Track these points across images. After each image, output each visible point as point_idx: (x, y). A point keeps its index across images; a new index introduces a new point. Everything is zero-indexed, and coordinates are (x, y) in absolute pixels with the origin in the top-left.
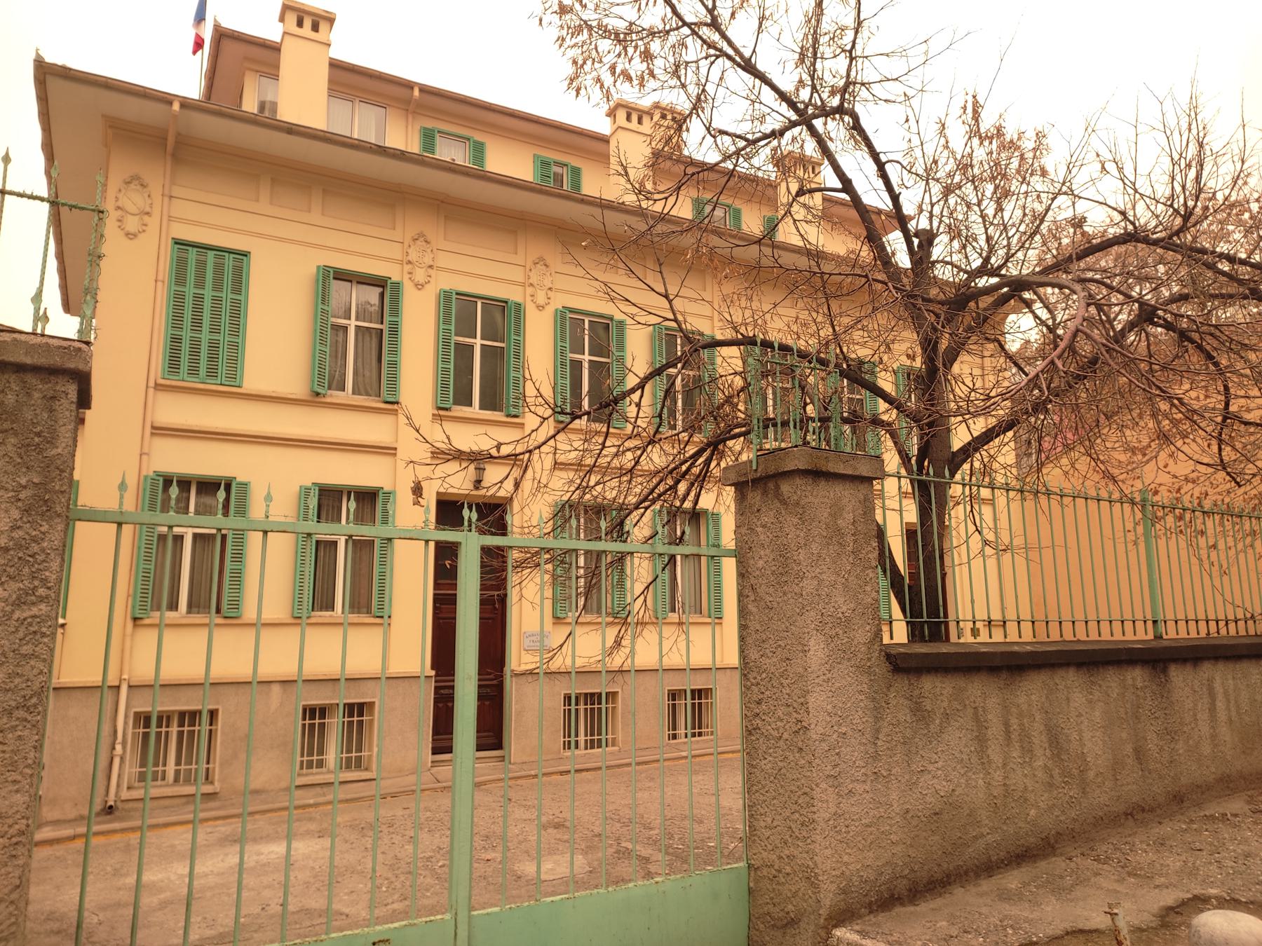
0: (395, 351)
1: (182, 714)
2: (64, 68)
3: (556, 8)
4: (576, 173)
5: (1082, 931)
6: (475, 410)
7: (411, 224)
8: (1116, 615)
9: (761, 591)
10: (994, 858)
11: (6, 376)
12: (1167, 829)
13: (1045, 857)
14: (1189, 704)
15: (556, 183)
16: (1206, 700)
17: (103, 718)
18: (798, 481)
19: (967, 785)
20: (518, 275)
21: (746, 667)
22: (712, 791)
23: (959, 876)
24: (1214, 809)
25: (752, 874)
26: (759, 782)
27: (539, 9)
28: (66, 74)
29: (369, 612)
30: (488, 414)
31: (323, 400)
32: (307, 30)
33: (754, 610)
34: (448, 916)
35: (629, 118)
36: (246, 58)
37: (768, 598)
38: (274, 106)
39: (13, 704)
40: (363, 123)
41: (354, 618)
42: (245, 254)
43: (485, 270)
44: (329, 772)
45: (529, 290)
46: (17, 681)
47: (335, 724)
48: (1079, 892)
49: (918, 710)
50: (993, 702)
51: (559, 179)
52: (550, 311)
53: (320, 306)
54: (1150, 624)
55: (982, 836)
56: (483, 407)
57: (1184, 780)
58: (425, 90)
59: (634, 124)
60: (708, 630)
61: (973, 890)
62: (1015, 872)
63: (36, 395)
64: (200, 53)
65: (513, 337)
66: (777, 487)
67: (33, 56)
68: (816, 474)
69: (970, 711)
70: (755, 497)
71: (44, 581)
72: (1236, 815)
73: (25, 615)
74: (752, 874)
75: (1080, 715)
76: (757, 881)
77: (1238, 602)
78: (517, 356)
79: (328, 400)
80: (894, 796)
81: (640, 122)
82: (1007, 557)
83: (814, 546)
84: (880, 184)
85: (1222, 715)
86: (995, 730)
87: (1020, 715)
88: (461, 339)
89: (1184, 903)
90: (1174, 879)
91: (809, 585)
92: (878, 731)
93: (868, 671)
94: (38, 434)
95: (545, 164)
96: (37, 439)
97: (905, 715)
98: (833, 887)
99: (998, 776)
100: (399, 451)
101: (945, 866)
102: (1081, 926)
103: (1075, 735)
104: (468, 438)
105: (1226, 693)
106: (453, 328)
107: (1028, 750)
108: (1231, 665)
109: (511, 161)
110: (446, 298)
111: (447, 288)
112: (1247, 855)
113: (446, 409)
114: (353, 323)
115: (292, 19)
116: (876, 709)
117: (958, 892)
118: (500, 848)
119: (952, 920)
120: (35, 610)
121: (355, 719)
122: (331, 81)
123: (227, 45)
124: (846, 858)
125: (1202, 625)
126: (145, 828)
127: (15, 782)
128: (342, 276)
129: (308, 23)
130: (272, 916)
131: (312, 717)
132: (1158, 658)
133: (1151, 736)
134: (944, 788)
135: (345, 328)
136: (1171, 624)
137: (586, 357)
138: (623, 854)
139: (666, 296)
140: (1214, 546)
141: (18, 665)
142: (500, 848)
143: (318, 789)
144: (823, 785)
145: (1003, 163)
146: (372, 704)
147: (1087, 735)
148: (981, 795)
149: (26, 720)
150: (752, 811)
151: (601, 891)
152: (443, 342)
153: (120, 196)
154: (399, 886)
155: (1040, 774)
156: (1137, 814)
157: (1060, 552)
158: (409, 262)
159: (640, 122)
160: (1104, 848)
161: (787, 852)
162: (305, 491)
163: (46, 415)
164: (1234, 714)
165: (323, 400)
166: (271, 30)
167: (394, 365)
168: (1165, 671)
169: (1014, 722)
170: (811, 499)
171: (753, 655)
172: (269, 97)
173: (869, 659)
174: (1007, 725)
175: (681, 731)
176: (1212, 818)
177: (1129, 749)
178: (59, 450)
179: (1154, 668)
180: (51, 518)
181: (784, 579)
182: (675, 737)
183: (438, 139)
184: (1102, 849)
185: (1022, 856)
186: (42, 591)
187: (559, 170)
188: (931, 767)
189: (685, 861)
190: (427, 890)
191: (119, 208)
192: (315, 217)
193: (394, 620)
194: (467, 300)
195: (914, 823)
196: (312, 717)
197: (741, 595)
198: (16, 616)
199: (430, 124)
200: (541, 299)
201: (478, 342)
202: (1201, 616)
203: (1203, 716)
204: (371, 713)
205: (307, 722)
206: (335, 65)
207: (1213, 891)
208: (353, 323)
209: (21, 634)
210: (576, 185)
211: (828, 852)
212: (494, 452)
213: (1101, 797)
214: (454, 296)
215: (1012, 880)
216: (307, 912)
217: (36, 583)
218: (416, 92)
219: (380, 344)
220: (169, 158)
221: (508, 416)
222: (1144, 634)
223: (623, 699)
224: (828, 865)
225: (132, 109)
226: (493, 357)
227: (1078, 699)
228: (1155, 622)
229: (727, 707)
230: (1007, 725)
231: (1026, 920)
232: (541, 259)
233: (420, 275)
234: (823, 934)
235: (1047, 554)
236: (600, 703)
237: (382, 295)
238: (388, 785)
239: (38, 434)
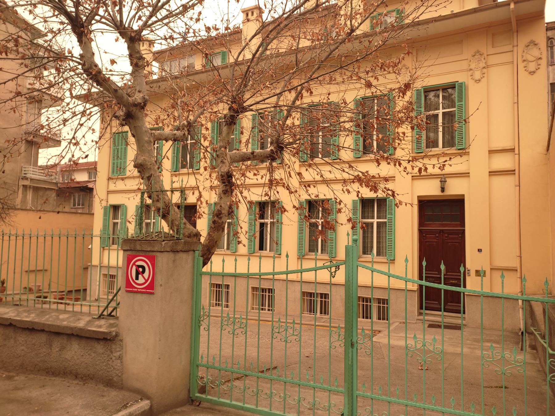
1: (321, 294)
17: (233, 288)
100: (471, 175)
191: (524, 61)
236: (314, 297)
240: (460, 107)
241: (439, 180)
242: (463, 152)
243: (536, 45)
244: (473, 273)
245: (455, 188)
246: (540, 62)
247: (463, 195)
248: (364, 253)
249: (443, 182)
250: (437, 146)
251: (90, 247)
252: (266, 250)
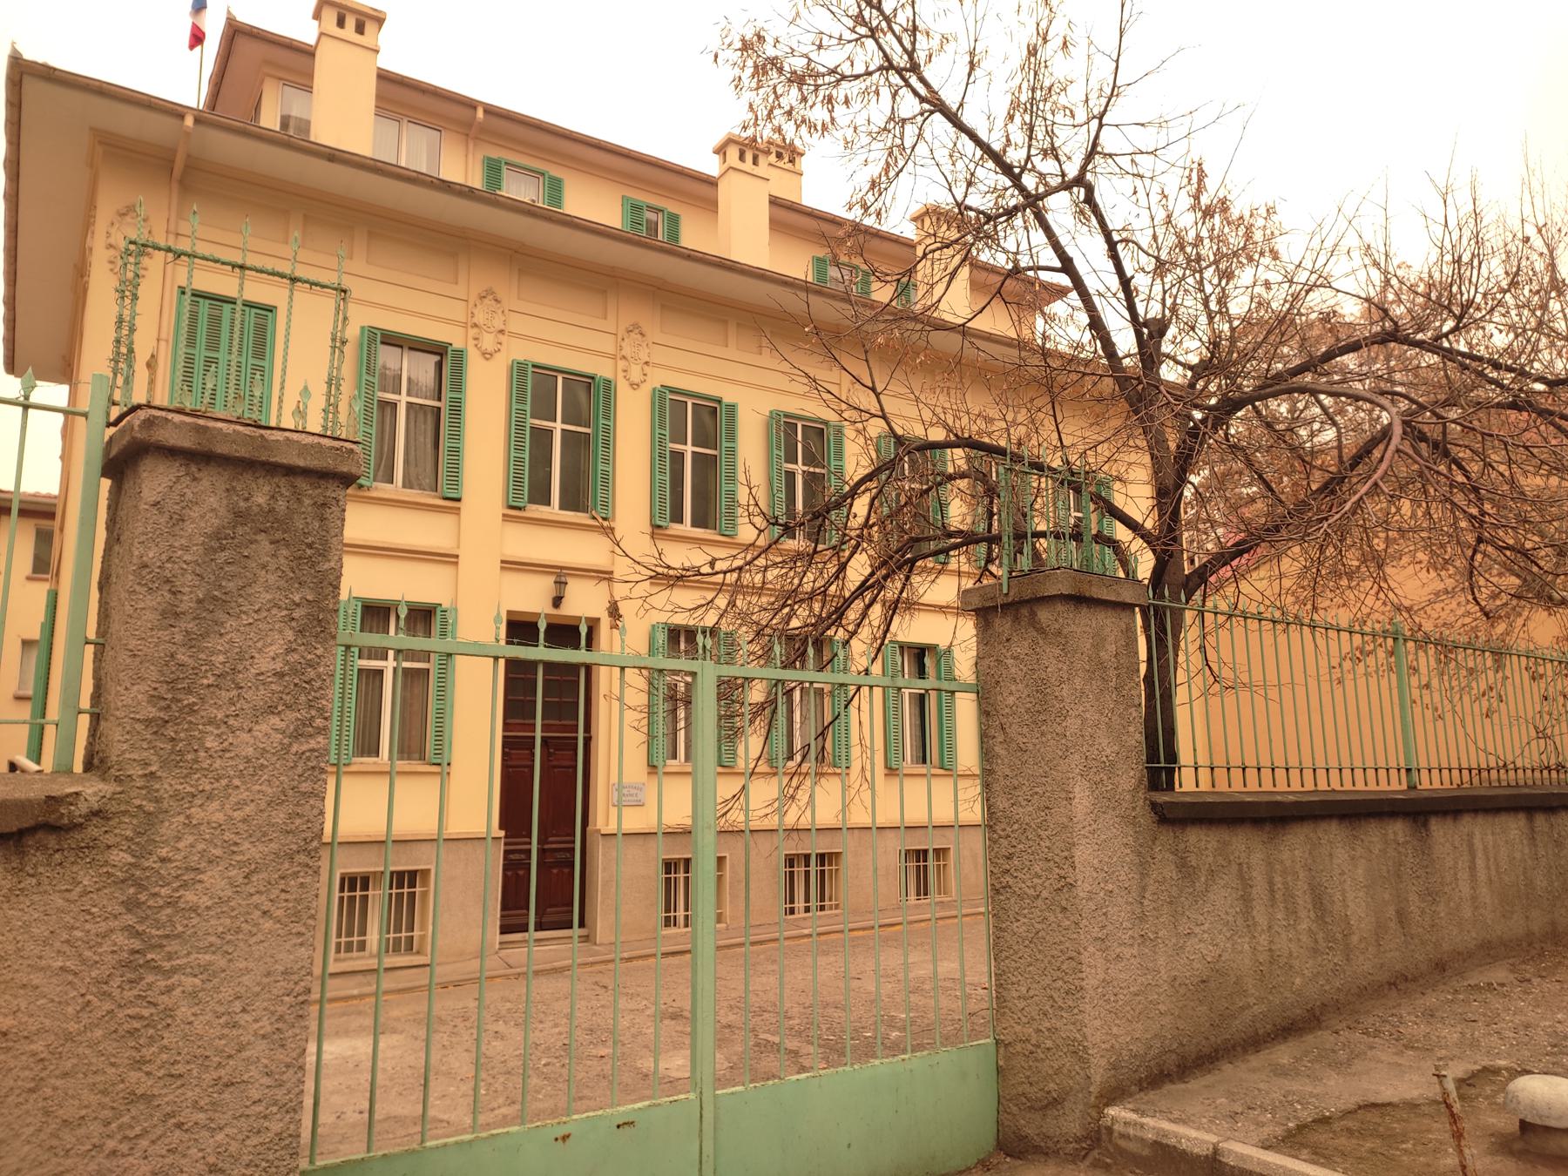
0: (457, 435)
2: (45, 66)
3: (739, 45)
4: (674, 220)
5: (1374, 1105)
6: (554, 510)
7: (478, 277)
8: (1370, 763)
9: (1013, 731)
10: (1261, 1032)
11: (276, 480)
12: (1431, 1000)
13: (1311, 1030)
14: (1449, 862)
15: (645, 232)
16: (1466, 857)
18: (1060, 607)
19: (1234, 949)
20: (608, 345)
21: (992, 819)
22: (951, 963)
23: (1227, 1050)
24: (1478, 978)
25: (1002, 1050)
26: (1010, 947)
27: (715, 45)
28: (49, 75)
29: (422, 757)
30: (699, 532)
31: (367, 494)
32: (349, 31)
33: (1003, 752)
34: (692, 1096)
35: (742, 158)
36: (268, 62)
37: (1021, 740)
38: (305, 126)
39: (294, 847)
40: (413, 149)
41: (402, 765)
42: (271, 309)
43: (570, 338)
44: (371, 956)
45: (621, 364)
46: (298, 821)
47: (378, 896)
48: (1358, 1065)
49: (1184, 867)
50: (1257, 858)
51: (653, 228)
52: (646, 390)
53: (365, 377)
54: (1403, 772)
55: (1249, 1006)
56: (694, 525)
57: (1446, 947)
58: (491, 111)
59: (748, 165)
61: (1243, 1066)
62: (1283, 1047)
63: (307, 502)
64: (198, 49)
65: (602, 421)
66: (1033, 614)
67: (7, 51)
68: (1079, 600)
69: (1235, 867)
70: (1003, 625)
71: (321, 710)
72: (1503, 985)
73: (304, 748)
74: (1002, 1050)
75: (1342, 873)
76: (1007, 1059)
77: (1491, 749)
78: (606, 445)
79: (374, 494)
80: (1161, 961)
81: (755, 162)
82: (1230, 698)
83: (1077, 680)
84: (1110, 266)
85: (1482, 875)
86: (1259, 889)
87: (1284, 872)
88: (537, 422)
89: (1474, 1075)
90: (1456, 1051)
91: (1073, 724)
92: (1144, 889)
93: (1133, 822)
94: (310, 546)
95: (636, 208)
96: (309, 552)
97: (1170, 872)
98: (1103, 1062)
99: (1263, 940)
100: (461, 560)
101: (1213, 1039)
102: (1372, 1100)
103: (1338, 896)
104: (679, 557)
105: (1485, 849)
106: (528, 408)
107: (1292, 912)
108: (1490, 819)
109: (594, 203)
110: (519, 370)
111: (521, 359)
112: (1527, 1027)
113: (519, 509)
114: (403, 399)
115: (330, 16)
116: (1141, 864)
117: (1227, 1068)
118: (610, 1043)
119: (1231, 1096)
120: (313, 744)
121: (406, 890)
122: (379, 97)
123: (243, 46)
124: (1115, 1030)
125: (1455, 773)
126: (531, 975)
127: (299, 934)
128: (392, 340)
129: (350, 22)
130: (354, 1126)
131: (352, 888)
132: (1418, 811)
133: (1413, 897)
134: (1211, 953)
135: (394, 405)
136: (1424, 773)
137: (689, 449)
138: (764, 1047)
139: (873, 389)
140: (1427, 686)
141: (298, 804)
142: (610, 1043)
143: (360, 978)
144: (1091, 949)
145: (1218, 240)
146: (425, 873)
147: (1350, 896)
148: (1247, 961)
149: (307, 865)
150: (1001, 981)
151: (848, 1068)
152: (515, 426)
153: (113, 231)
154: (500, 1088)
155: (1304, 938)
156: (1400, 983)
157: (1300, 691)
158: (475, 325)
159: (755, 162)
160: (1371, 1020)
161: (1048, 1025)
163: (317, 524)
164: (1493, 873)
165: (367, 494)
166: (304, 30)
167: (456, 452)
168: (1425, 824)
169: (1278, 879)
170: (1073, 628)
171: (1001, 803)
172: (295, 112)
173: (1134, 809)
174: (1271, 883)
175: (800, 904)
176: (1476, 988)
177: (1391, 911)
178: (332, 564)
179: (1415, 821)
180: (326, 640)
181: (1042, 717)
182: (792, 911)
183: (505, 171)
184: (1368, 1021)
185: (1288, 1030)
186: (319, 722)
187: (652, 216)
188: (1197, 930)
189: (843, 1054)
190: (538, 1092)
193: (454, 769)
194: (546, 375)
195: (1182, 990)
196: (352, 888)
197: (984, 736)
198: (294, 750)
199: (496, 153)
200: (636, 376)
201: (558, 427)
202: (1455, 764)
203: (1464, 875)
204: (425, 883)
205: (346, 894)
206: (384, 77)
207: (1502, 1063)
208: (403, 399)
209: (299, 770)
210: (674, 234)
211: (1098, 1023)
212: (706, 569)
213: (1365, 965)
214: (530, 369)
215: (1283, 1054)
216: (397, 1119)
217: (313, 713)
218: (480, 114)
219: (438, 425)
220: (175, 186)
222: (1396, 785)
223: (732, 866)
224: (1098, 1037)
225: (129, 123)
226: (706, 465)
227: (1341, 855)
228: (1409, 770)
229: (968, 866)
230: (1271, 883)
231: (1311, 1095)
232: (636, 326)
233: (488, 342)
234: (1094, 1114)
235: (1287, 691)
237: (439, 366)
238: (444, 972)
239: (310, 546)
245: (583, 602)
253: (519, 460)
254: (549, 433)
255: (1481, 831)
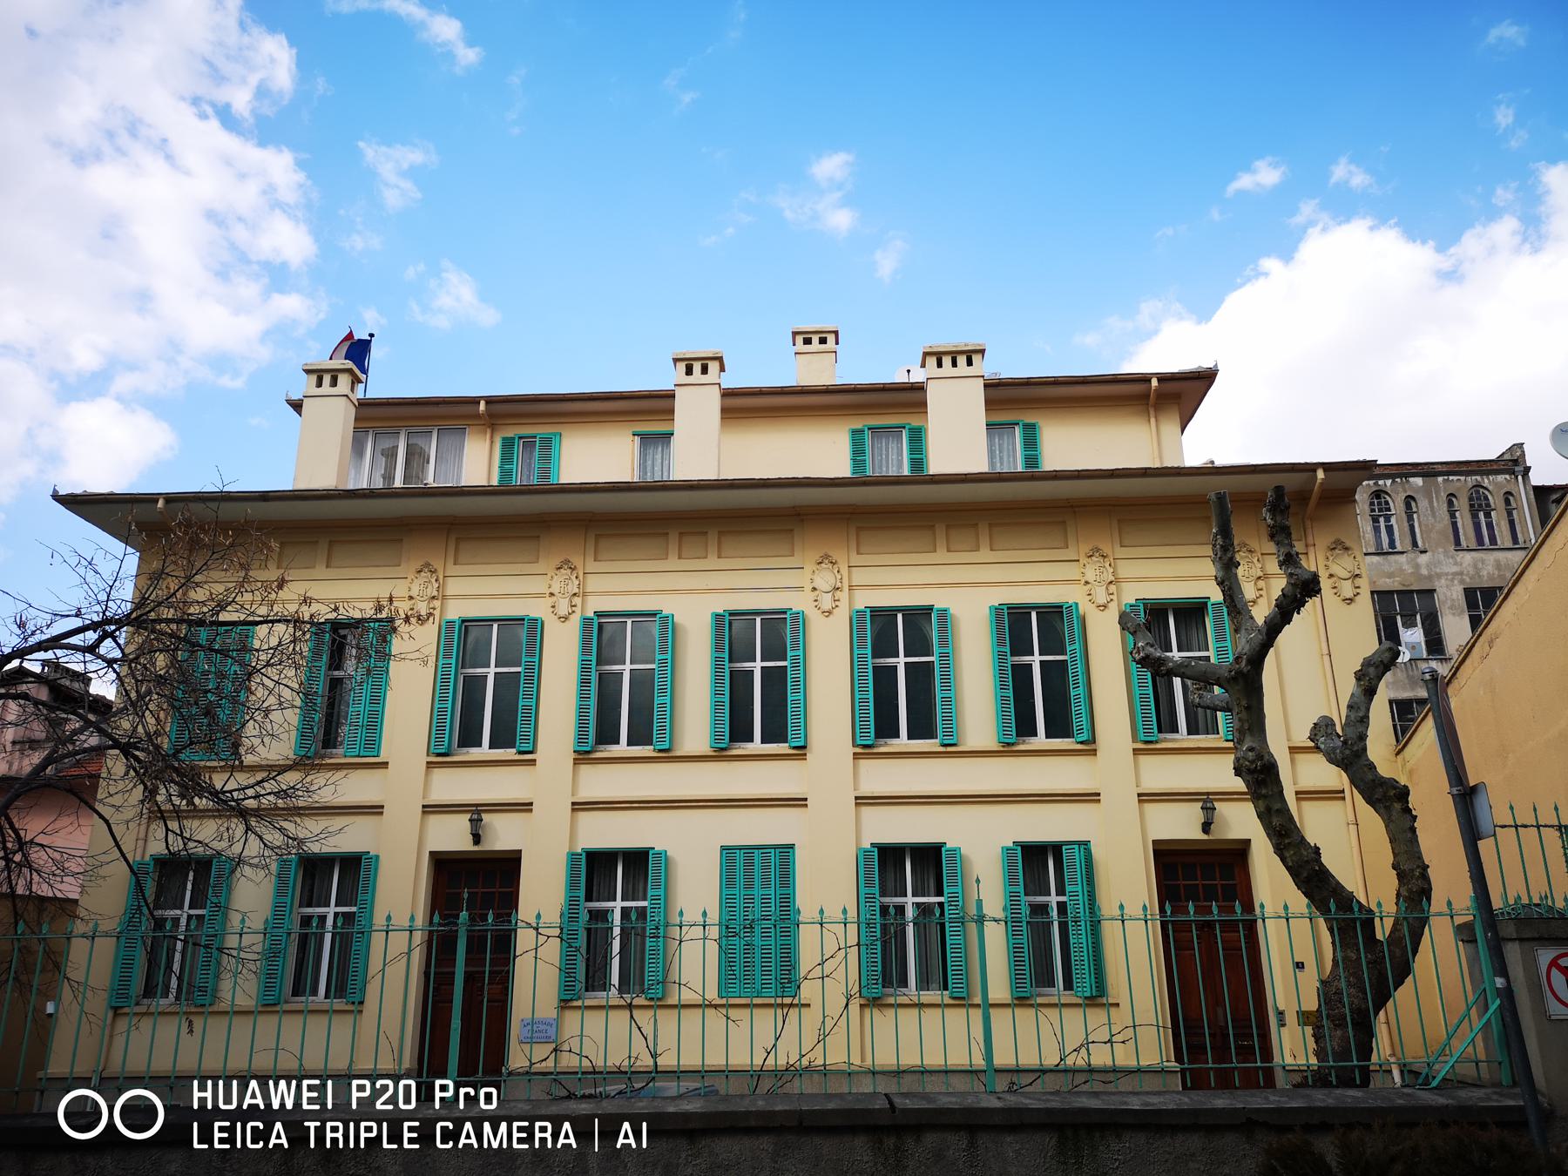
6: (1041, 740)
30: (500, 754)
52: (576, 619)
56: (912, 736)
59: (326, 388)
60: (349, 1019)
106: (869, 651)
162: (1008, 851)
191: (1331, 576)
192: (712, 562)
221: (521, 753)
226: (775, 679)
240: (944, 656)
241: (1200, 804)
242: (527, 759)
243: (1347, 549)
244: (1291, 1018)
245: (503, 834)
246: (1358, 581)
247: (520, 852)
248: (297, 991)
249: (476, 823)
250: (751, 740)
251: (50, 1008)
252: (315, 992)
253: (442, 711)
254: (1028, 668)
255: (1011, 1144)
